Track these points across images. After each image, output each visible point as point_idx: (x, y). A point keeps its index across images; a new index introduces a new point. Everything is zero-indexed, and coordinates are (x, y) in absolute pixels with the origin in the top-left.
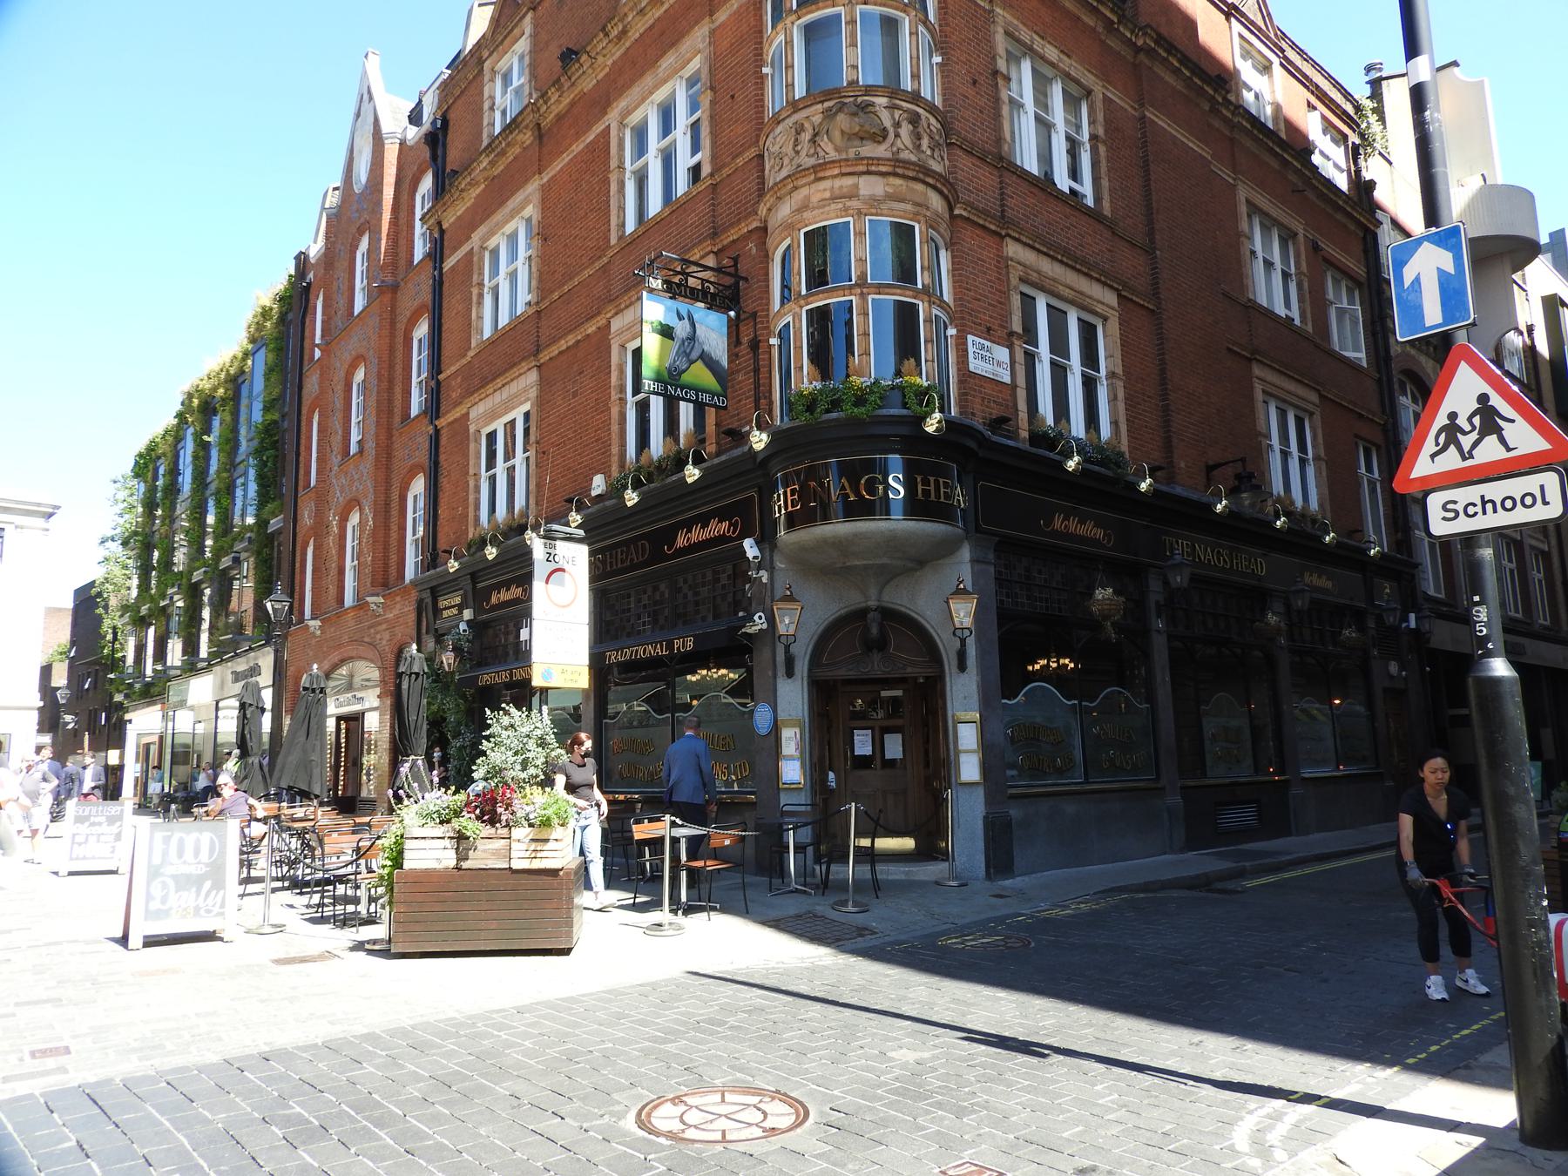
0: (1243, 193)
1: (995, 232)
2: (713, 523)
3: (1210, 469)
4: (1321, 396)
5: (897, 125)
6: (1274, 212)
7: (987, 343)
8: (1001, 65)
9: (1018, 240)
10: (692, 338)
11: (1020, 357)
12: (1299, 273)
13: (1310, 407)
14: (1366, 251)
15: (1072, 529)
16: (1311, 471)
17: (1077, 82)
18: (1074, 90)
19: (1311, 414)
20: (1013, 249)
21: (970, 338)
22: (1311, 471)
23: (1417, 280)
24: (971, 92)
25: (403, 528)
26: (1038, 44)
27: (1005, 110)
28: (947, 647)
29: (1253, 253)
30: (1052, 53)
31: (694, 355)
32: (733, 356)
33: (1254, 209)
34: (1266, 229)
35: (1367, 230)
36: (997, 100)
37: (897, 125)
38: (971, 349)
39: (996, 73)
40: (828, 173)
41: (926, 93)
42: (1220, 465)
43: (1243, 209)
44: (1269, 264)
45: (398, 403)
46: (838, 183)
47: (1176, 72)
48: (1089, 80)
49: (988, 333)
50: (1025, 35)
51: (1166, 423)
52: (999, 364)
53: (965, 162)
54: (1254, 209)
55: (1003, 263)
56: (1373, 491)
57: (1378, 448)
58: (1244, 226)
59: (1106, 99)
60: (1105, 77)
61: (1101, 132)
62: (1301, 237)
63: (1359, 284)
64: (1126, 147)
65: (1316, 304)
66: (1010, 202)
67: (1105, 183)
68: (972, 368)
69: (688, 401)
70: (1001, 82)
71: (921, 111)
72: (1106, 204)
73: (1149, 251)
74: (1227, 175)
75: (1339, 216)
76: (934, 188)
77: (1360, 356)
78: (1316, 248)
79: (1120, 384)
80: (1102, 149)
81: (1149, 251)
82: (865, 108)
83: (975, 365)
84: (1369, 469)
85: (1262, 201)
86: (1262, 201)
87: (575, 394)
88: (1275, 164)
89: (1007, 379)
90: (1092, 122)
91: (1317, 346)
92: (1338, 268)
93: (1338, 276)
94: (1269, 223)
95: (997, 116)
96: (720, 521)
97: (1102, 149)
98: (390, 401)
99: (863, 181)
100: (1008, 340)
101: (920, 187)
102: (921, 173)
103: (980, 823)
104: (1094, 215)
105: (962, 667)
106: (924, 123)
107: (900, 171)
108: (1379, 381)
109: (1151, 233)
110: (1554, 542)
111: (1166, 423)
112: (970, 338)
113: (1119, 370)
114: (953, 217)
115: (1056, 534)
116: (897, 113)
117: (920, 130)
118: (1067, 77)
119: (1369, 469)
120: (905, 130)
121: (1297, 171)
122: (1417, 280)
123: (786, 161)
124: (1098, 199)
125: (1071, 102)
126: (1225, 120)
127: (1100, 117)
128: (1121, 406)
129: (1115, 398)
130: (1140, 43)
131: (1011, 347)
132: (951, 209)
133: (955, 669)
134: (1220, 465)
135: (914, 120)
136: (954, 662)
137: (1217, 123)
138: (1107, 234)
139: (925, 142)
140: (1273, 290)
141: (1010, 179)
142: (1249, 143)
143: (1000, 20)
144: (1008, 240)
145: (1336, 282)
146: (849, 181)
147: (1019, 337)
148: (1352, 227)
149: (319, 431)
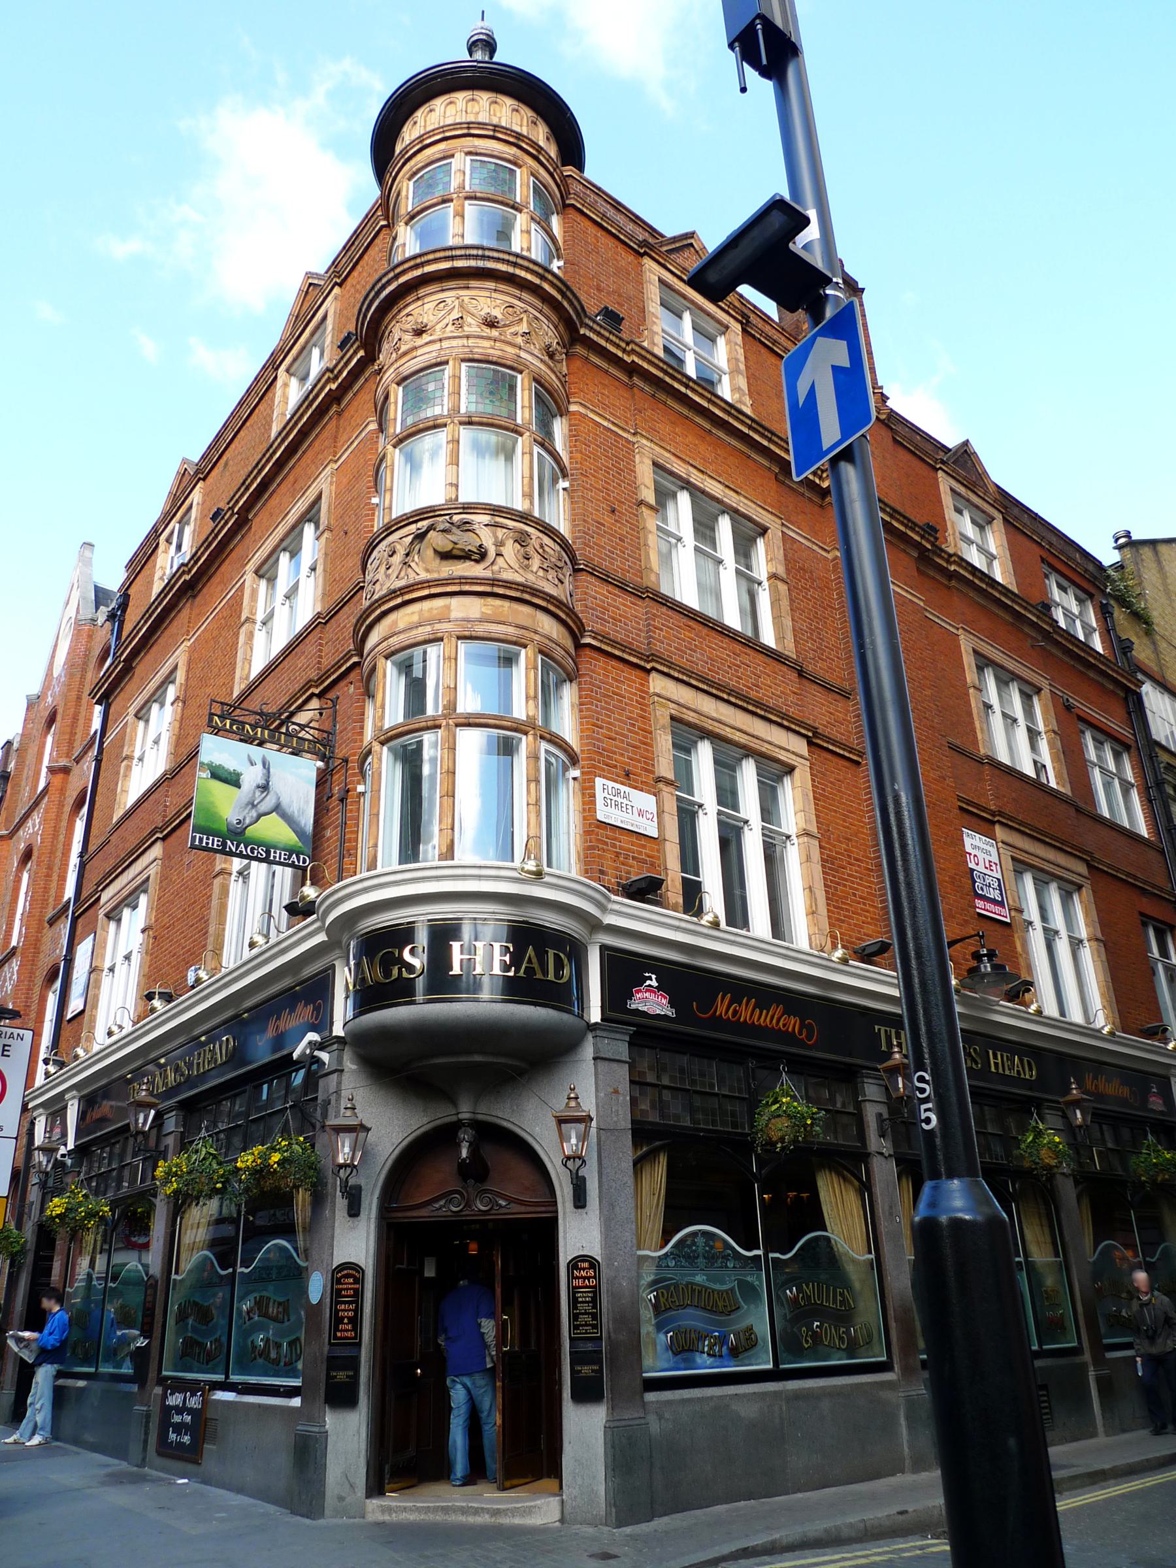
0: (966, 644)
4: (1090, 867)
5: (500, 544)
6: (1010, 665)
7: (623, 788)
10: (265, 788)
11: (671, 806)
13: (1075, 878)
20: (657, 684)
21: (599, 782)
24: (608, 519)
26: (696, 478)
29: (988, 707)
33: (983, 662)
34: (1002, 683)
35: (1128, 690)
37: (500, 544)
38: (600, 795)
40: (511, 630)
41: (768, 637)
43: (969, 660)
46: (426, 605)
49: (627, 777)
52: (641, 813)
58: (971, 676)
75: (1091, 674)
82: (466, 527)
83: (604, 813)
91: (1078, 810)
93: (1101, 737)
94: (1005, 679)
99: (455, 602)
100: (653, 784)
102: (525, 595)
103: (600, 1435)
105: (580, 1201)
106: (534, 542)
112: (599, 782)
115: (717, 1023)
116: (500, 533)
117: (530, 549)
118: (734, 513)
120: (510, 550)
124: (780, 638)
132: (576, 639)
133: (569, 1204)
135: (522, 540)
138: (793, 676)
145: (1099, 744)
147: (669, 783)
149: (260, 1405)
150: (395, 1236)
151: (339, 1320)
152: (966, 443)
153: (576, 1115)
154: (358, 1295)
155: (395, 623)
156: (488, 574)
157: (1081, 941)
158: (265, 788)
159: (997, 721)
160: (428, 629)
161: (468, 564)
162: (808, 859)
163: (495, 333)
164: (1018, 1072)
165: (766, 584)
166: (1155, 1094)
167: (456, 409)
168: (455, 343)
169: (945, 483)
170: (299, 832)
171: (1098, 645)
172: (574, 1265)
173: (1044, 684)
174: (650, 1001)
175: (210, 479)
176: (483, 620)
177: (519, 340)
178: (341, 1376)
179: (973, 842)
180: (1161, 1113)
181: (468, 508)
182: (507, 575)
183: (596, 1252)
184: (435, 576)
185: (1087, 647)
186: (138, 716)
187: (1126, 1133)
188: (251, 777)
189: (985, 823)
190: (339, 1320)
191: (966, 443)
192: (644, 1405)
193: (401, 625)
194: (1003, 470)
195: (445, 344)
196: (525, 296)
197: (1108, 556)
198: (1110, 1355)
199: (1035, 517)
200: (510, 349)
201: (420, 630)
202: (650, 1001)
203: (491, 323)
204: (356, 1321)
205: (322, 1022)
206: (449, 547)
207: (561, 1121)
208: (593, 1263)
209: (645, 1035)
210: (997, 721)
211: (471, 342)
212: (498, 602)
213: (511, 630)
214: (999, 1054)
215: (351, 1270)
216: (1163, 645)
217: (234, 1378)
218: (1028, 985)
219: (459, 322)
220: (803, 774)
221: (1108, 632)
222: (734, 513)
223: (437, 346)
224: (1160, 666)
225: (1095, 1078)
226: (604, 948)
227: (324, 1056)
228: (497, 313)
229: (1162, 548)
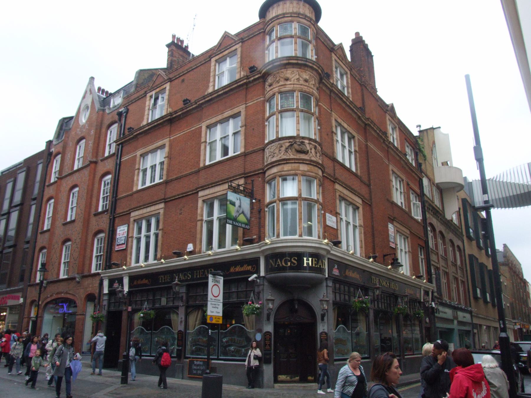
0: (391, 167)
1: (333, 181)
2: (245, 266)
3: (385, 256)
4: (410, 232)
5: (311, 149)
6: (398, 173)
8: (334, 130)
9: (338, 183)
10: (240, 206)
12: (404, 192)
13: (407, 235)
14: (420, 185)
15: (351, 275)
16: (357, 231)
17: (351, 134)
18: (350, 136)
19: (407, 237)
20: (337, 186)
22: (357, 231)
23: (505, 246)
25: (92, 251)
27: (335, 143)
28: (318, 313)
30: (345, 125)
31: (241, 212)
32: (251, 213)
34: (396, 178)
36: (333, 140)
37: (311, 149)
38: (327, 218)
39: (333, 132)
40: (314, 174)
41: (354, 169)
42: (388, 255)
44: (397, 189)
45: (94, 204)
46: (293, 165)
47: (375, 131)
48: (354, 133)
50: (339, 120)
51: (373, 242)
53: (326, 159)
54: (394, 172)
55: (335, 190)
56: (422, 262)
57: (423, 248)
59: (358, 139)
60: (358, 133)
61: (357, 149)
62: (404, 181)
63: (418, 195)
64: (364, 155)
65: (408, 200)
66: (336, 171)
67: (358, 165)
68: (327, 224)
69: (230, 224)
70: (334, 135)
71: (317, 145)
72: (359, 172)
73: (369, 186)
74: (386, 161)
75: (413, 174)
76: (320, 168)
77: (419, 218)
78: (408, 184)
79: (362, 229)
80: (358, 154)
81: (369, 186)
82: (302, 143)
84: (421, 255)
85: (395, 170)
86: (395, 170)
87: (181, 214)
88: (398, 158)
89: (335, 227)
90: (355, 146)
92: (414, 191)
94: (397, 177)
95: (333, 145)
96: (248, 266)
97: (358, 154)
98: (91, 203)
99: (301, 165)
101: (316, 168)
104: (355, 175)
107: (312, 163)
108: (424, 227)
109: (369, 181)
110: (466, 278)
111: (373, 242)
112: (327, 214)
113: (362, 224)
114: (323, 176)
116: (311, 146)
119: (421, 255)
120: (313, 150)
121: (404, 161)
122: (505, 246)
123: (276, 155)
124: (356, 170)
125: (350, 139)
126: (387, 145)
127: (357, 144)
128: (363, 235)
129: (361, 233)
130: (367, 122)
131: (336, 217)
133: (320, 321)
134: (388, 255)
135: (315, 148)
136: (320, 319)
137: (384, 146)
138: (359, 180)
139: (318, 155)
140: (398, 198)
141: (336, 164)
142: (392, 152)
143: (333, 116)
144: (336, 184)
146: (297, 165)
148: (416, 177)
150: (276, 326)
151: (266, 345)
152: (341, 44)
153: (322, 299)
154: (270, 339)
155: (283, 168)
156: (308, 158)
157: (356, 226)
158: (240, 206)
159: (394, 189)
160: (294, 172)
161: (303, 155)
162: (361, 233)
163: (307, 84)
164: (320, 266)
165: (353, 153)
166: (336, 269)
167: (297, 107)
168: (298, 86)
169: (388, 117)
170: (247, 219)
171: (414, 165)
172: (321, 333)
173: (404, 178)
174: (336, 272)
175: (173, 83)
176: (308, 171)
177: (312, 86)
178: (268, 357)
179: (390, 226)
180: (337, 276)
181: (303, 138)
182: (313, 159)
183: (326, 331)
184: (295, 157)
185: (411, 164)
186: (141, 155)
187: (352, 289)
188: (237, 203)
189: (392, 220)
190: (266, 345)
191: (341, 44)
192: (334, 365)
193: (285, 169)
194: (400, 114)
195: (295, 86)
196: (314, 72)
197: (416, 133)
198: (406, 357)
199: (404, 126)
200: (311, 90)
201: (292, 172)
202: (336, 272)
203: (306, 81)
204: (270, 345)
205: (257, 271)
206: (300, 149)
207: (321, 301)
208: (326, 334)
209: (335, 280)
210: (394, 189)
211: (302, 86)
212: (311, 166)
213: (314, 174)
214: (310, 259)
215: (268, 333)
216: (427, 163)
217: (220, 357)
218: (340, 242)
219: (298, 80)
220: (361, 209)
221: (416, 160)
222: (349, 132)
223: (292, 86)
224: (426, 169)
225: (349, 271)
226: (329, 259)
227: (258, 281)
228: (307, 77)
229: (429, 131)
